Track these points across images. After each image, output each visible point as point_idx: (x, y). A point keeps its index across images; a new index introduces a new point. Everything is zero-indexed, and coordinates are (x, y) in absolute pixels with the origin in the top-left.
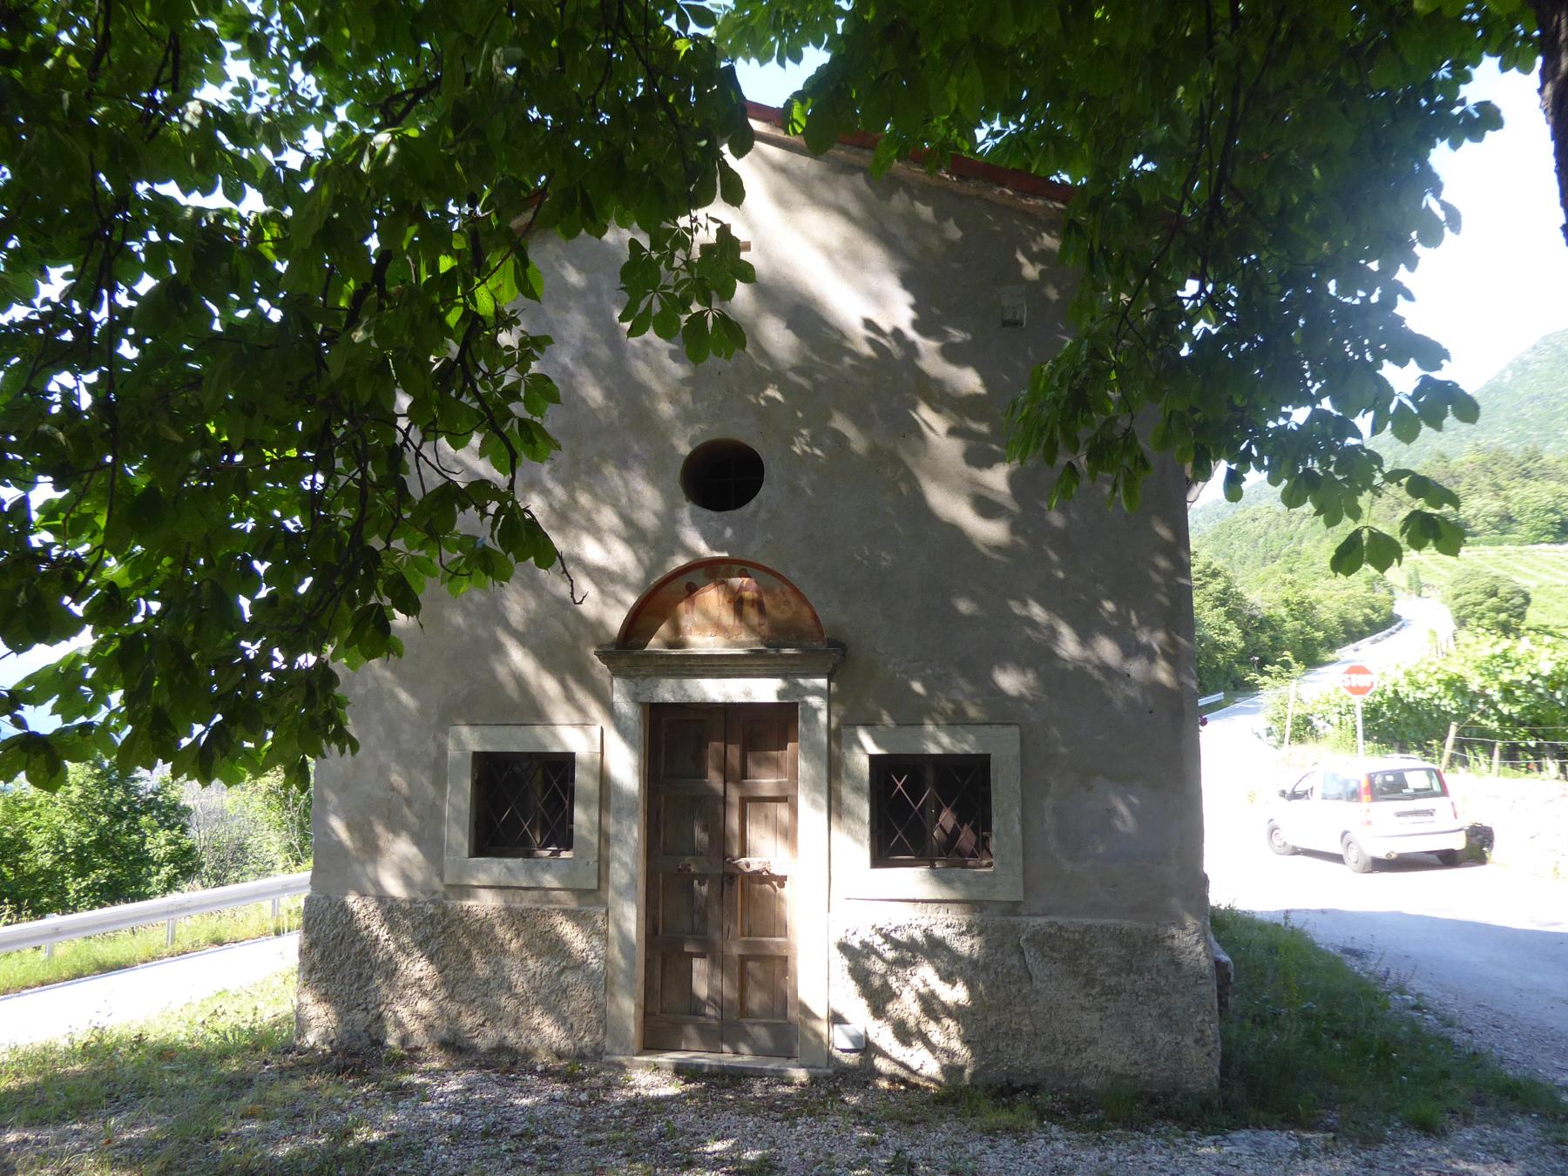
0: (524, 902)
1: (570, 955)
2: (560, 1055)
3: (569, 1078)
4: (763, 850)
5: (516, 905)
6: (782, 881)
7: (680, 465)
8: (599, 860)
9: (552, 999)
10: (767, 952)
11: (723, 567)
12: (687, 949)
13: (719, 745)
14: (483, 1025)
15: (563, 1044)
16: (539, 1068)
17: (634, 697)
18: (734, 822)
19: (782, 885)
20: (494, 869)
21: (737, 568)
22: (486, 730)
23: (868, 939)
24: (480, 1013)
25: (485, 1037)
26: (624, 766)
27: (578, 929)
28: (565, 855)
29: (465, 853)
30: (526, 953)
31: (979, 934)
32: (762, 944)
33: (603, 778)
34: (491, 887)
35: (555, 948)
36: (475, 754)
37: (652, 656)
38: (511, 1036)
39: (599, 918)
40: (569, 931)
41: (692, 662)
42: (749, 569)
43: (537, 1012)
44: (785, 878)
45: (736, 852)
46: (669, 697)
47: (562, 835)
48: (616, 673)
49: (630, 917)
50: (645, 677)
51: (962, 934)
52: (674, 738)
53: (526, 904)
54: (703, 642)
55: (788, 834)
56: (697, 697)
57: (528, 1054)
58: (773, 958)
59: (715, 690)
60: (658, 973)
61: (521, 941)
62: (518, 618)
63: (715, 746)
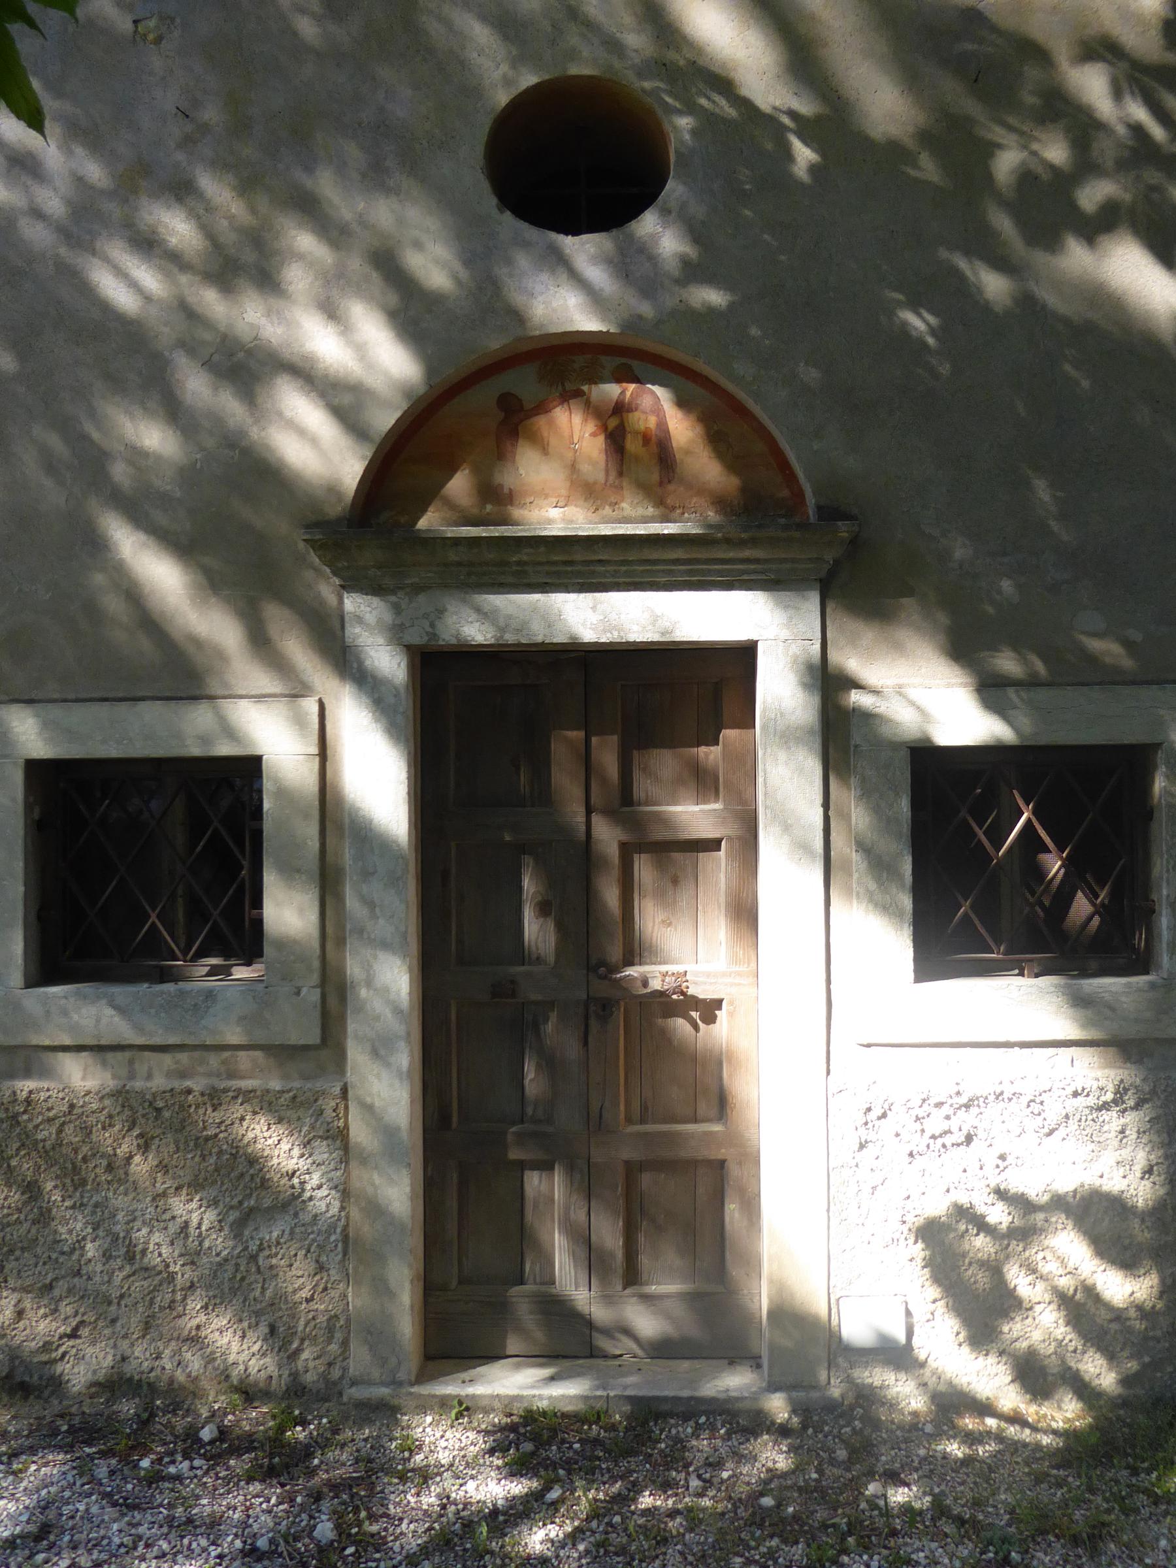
0: (156, 1077)
1: (265, 1184)
2: (248, 1393)
3: (279, 1462)
4: (686, 950)
5: (138, 1084)
6: (710, 1009)
7: (483, 126)
8: (324, 982)
9: (237, 1283)
10: (684, 1154)
11: (580, 361)
12: (514, 1154)
13: (577, 735)
14: (74, 1335)
15: (254, 1365)
16: (206, 1434)
17: (396, 634)
18: (611, 896)
19: (710, 1019)
20: (87, 1009)
21: (609, 363)
22: (56, 711)
23: (1139, 1175)
24: (66, 1309)
25: (80, 1358)
26: (378, 781)
27: (281, 1129)
28: (241, 973)
29: (16, 977)
30: (163, 1183)
31: (1137, 1107)
32: (671, 1137)
33: (328, 802)
34: (80, 1048)
35: (244, 1187)
36: (35, 769)
37: (431, 542)
38: (140, 1354)
39: (329, 1105)
40: (279, 1148)
41: (524, 555)
42: (635, 364)
43: (195, 1304)
44: (718, 1003)
45: (615, 953)
46: (477, 633)
47: (244, 937)
48: (353, 583)
49: (385, 1089)
50: (418, 589)
51: (1105, 1106)
52: (472, 718)
53: (159, 1082)
54: (554, 513)
55: (745, 914)
56: (539, 634)
57: (178, 1397)
58: (690, 1166)
59: (590, 617)
60: (452, 1204)
61: (152, 1160)
62: (40, 744)
63: (564, 743)
